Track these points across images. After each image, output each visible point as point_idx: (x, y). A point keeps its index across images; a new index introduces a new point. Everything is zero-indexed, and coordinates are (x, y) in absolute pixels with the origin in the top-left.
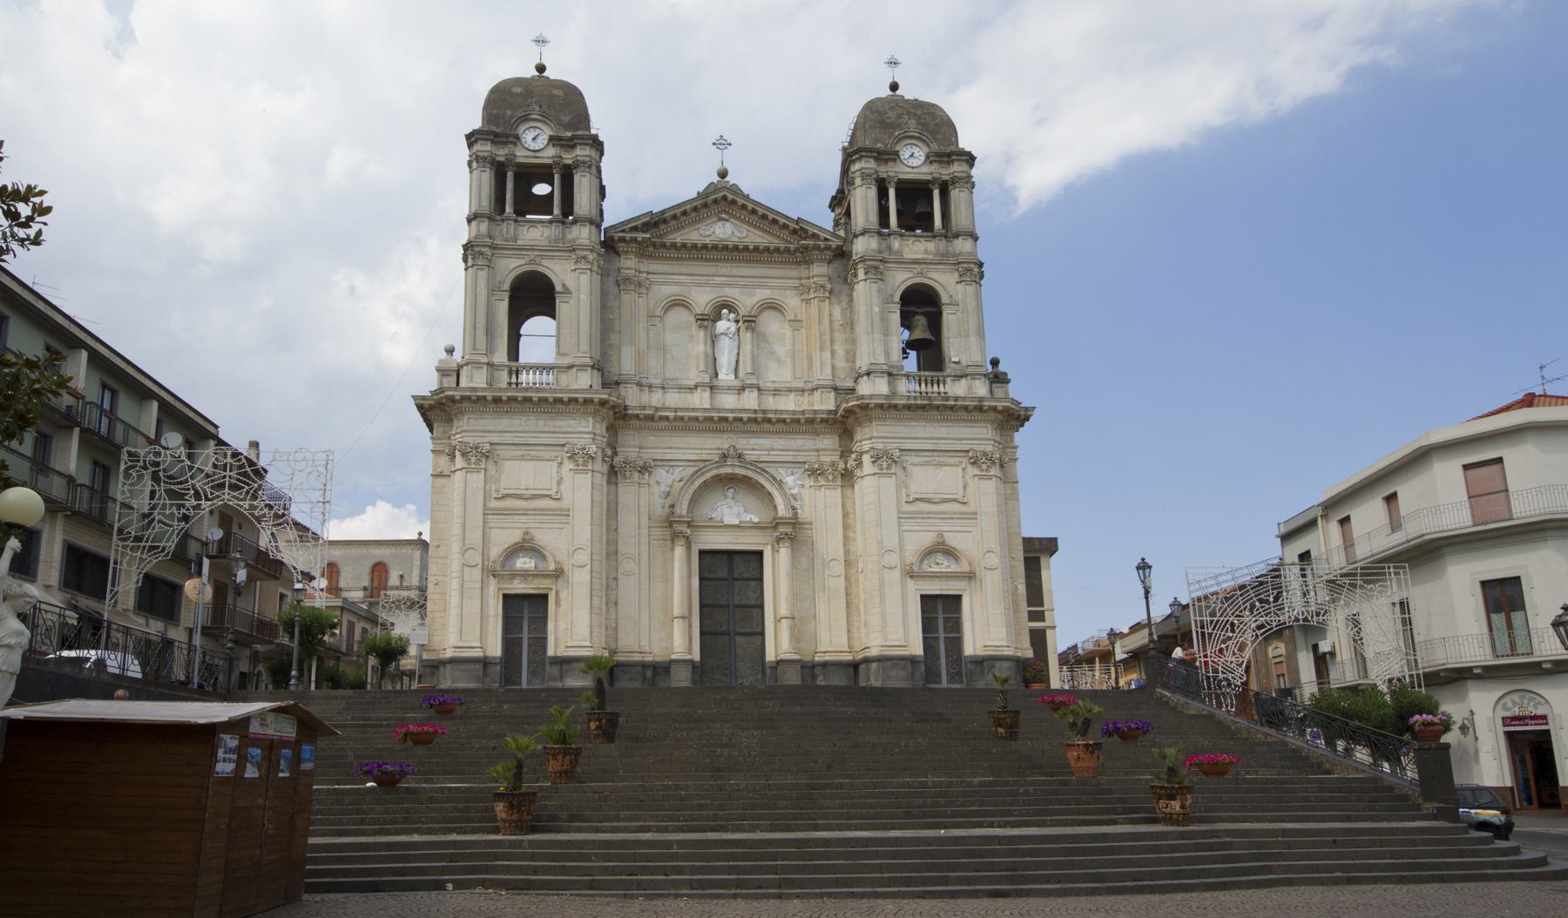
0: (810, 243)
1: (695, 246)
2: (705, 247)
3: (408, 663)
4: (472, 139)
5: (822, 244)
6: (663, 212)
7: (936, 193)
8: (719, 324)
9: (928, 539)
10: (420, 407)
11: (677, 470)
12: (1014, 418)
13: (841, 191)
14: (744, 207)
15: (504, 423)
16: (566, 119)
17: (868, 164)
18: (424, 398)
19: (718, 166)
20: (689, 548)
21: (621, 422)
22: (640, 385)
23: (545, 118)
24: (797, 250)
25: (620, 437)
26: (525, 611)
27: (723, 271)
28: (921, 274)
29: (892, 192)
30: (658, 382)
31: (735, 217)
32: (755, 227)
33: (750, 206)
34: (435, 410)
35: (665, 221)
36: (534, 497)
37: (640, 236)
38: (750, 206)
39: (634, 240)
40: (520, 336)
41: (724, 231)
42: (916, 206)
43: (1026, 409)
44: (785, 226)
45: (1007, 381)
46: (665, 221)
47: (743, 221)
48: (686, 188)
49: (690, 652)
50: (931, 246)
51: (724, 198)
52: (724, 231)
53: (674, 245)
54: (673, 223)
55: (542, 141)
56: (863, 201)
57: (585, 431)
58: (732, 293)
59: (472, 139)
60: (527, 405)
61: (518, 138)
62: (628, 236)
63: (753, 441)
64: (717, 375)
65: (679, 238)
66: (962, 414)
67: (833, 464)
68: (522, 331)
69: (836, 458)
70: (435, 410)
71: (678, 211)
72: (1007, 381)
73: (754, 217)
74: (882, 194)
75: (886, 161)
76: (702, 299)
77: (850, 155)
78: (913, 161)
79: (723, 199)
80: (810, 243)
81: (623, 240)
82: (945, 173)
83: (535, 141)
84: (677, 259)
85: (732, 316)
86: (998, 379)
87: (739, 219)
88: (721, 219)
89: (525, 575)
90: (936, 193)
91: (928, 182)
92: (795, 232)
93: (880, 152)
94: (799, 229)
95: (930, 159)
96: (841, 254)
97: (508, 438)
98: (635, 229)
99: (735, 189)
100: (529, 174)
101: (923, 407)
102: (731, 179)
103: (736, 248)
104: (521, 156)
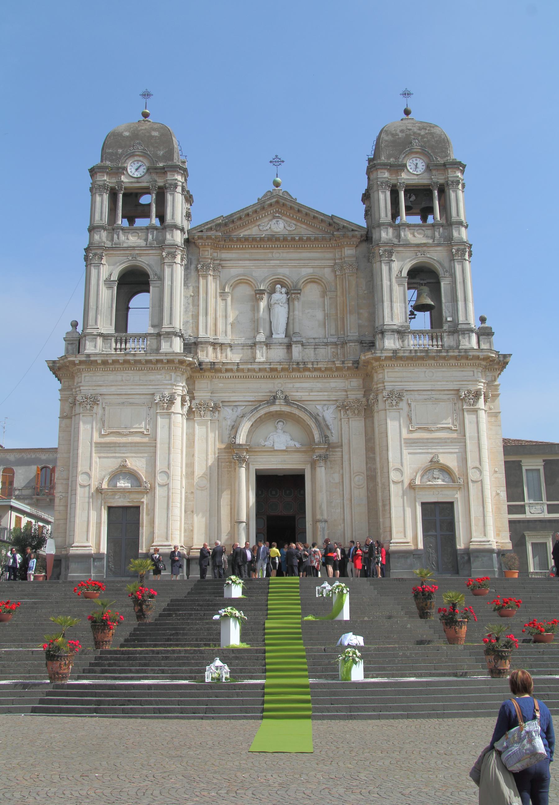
1: (254, 239)
2: (262, 240)
4: (93, 172)
6: (232, 215)
7: (436, 193)
8: (274, 295)
9: (424, 460)
10: (51, 369)
11: (240, 409)
12: (499, 363)
13: (367, 190)
15: (111, 377)
16: (161, 153)
17: (385, 175)
18: (54, 362)
20: (248, 469)
21: (198, 375)
22: (214, 344)
23: (144, 155)
25: (197, 385)
26: (125, 521)
27: (276, 255)
29: (402, 194)
31: (285, 215)
32: (301, 222)
34: (58, 368)
36: (391, 301)
37: (212, 233)
38: (296, 207)
39: (209, 238)
40: (128, 308)
41: (279, 226)
42: (422, 200)
43: (505, 356)
45: (492, 334)
47: (292, 218)
48: (248, 199)
52: (279, 226)
53: (239, 240)
54: (239, 223)
55: (142, 170)
56: (383, 199)
57: (250, 342)
58: (284, 272)
59: (93, 172)
60: (126, 366)
62: (205, 234)
63: (297, 385)
64: (272, 334)
65: (244, 233)
67: (358, 400)
68: (131, 305)
70: (58, 368)
72: (492, 334)
73: (299, 215)
74: (395, 194)
77: (373, 166)
78: (415, 171)
79: (278, 203)
81: (200, 238)
82: (439, 178)
84: (243, 249)
85: (284, 290)
86: (485, 333)
87: (289, 217)
88: (274, 217)
89: (124, 491)
90: (436, 193)
91: (429, 185)
93: (391, 166)
95: (429, 168)
96: (367, 238)
100: (132, 196)
101: (422, 358)
103: (285, 239)
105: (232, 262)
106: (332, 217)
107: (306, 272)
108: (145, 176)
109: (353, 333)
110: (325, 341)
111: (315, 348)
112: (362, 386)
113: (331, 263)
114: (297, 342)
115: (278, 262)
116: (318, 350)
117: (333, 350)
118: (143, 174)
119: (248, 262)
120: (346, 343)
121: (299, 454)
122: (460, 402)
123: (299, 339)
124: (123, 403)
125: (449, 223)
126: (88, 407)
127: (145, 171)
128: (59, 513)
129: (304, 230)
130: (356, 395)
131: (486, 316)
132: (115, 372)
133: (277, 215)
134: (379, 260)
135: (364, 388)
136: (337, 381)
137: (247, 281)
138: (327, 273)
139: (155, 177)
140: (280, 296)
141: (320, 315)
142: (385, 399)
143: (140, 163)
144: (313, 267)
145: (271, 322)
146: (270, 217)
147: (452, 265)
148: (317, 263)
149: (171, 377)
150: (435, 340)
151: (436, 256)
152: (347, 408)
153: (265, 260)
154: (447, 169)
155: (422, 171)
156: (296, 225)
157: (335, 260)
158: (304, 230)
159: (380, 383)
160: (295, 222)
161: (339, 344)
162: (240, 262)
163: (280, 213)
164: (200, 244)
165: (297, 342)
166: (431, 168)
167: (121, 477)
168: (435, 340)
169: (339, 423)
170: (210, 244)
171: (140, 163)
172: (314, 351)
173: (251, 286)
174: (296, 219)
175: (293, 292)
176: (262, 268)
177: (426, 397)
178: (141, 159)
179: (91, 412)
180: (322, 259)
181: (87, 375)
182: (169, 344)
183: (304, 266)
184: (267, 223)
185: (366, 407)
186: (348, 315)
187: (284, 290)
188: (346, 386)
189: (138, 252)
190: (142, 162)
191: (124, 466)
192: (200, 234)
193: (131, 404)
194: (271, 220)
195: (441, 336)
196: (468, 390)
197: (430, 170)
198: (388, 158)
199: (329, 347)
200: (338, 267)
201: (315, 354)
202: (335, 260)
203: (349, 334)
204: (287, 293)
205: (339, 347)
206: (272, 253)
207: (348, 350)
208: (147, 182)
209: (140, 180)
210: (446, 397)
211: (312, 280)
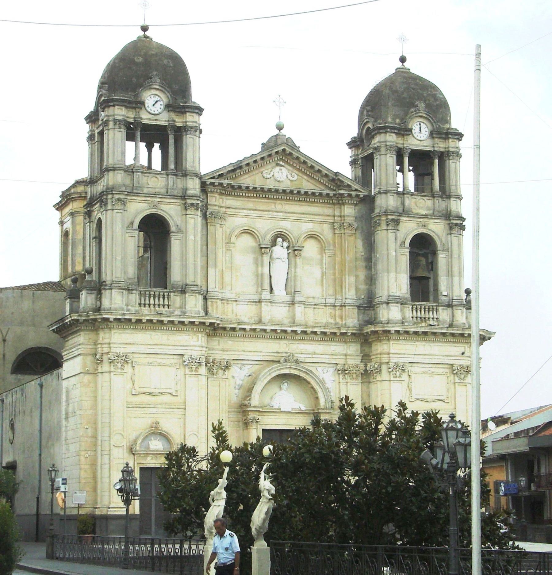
0: (346, 193)
3: (448, 526)
5: (354, 194)
14: (298, 158)
19: (276, 121)
24: (335, 195)
28: (424, 226)
30: (232, 296)
31: (289, 164)
33: (302, 159)
35: (241, 167)
39: (221, 184)
41: (282, 176)
44: (326, 176)
46: (241, 167)
49: (113, 503)
50: (429, 202)
51: (284, 150)
52: (282, 176)
55: (159, 108)
58: (286, 226)
61: (143, 103)
62: (217, 182)
66: (450, 339)
67: (357, 366)
69: (358, 362)
71: (251, 161)
75: (403, 135)
76: (265, 226)
80: (346, 193)
81: (212, 184)
82: (440, 145)
83: (154, 105)
85: (285, 244)
87: (292, 166)
88: (278, 165)
92: (333, 180)
94: (336, 180)
97: (143, 349)
98: (221, 176)
99: (289, 142)
102: (287, 132)
104: (146, 118)
105: (237, 211)
106: (337, 174)
107: (308, 227)
108: (163, 114)
109: (350, 294)
110: (324, 301)
111: (314, 308)
112: (359, 352)
113: (330, 219)
114: (300, 303)
115: (281, 214)
116: (316, 309)
117: (330, 311)
118: (160, 111)
119: (252, 212)
120: (345, 306)
121: (301, 415)
122: (452, 376)
123: (302, 299)
124: (152, 363)
125: (446, 193)
126: (119, 365)
127: (162, 107)
128: (85, 471)
129: (308, 185)
130: (355, 361)
131: (471, 289)
132: (144, 330)
133: (281, 163)
134: (385, 228)
135: (361, 352)
136: (337, 344)
137: (249, 231)
138: (326, 231)
139: (173, 115)
140: (280, 251)
141: (317, 273)
142: (390, 370)
143: (157, 98)
144: (313, 222)
145: (271, 277)
146: (274, 164)
147: (449, 238)
148: (316, 218)
149: (198, 338)
150: (431, 313)
151: (436, 228)
152: (346, 372)
153: (269, 211)
154: (448, 138)
155: (425, 137)
156: (298, 175)
157: (334, 216)
158: (308, 185)
159: (385, 354)
160: (297, 172)
161: (337, 306)
162: (245, 211)
163: (284, 161)
164: (210, 190)
165: (300, 303)
166: (434, 136)
167: (152, 438)
168: (431, 313)
169: (338, 386)
170: (218, 191)
171: (157, 98)
172: (314, 311)
173: (255, 238)
174: (298, 170)
175: (294, 251)
176: (266, 219)
177: (424, 369)
178: (157, 92)
179: (122, 371)
180: (323, 215)
181: (116, 331)
182: (184, 297)
183: (305, 221)
184: (270, 170)
185: (363, 372)
186: (347, 277)
187: (285, 244)
188: (350, 353)
189: (159, 200)
190: (159, 96)
191: (157, 428)
192: (212, 181)
193: (160, 365)
194: (273, 168)
195: (437, 309)
196: (460, 365)
197: (433, 137)
198: (394, 119)
199: (327, 307)
200: (338, 226)
201: (314, 314)
202: (334, 216)
203: (347, 297)
204: (288, 248)
205: (337, 308)
206: (275, 203)
207: (347, 313)
208: (166, 121)
209: (158, 117)
210: (441, 370)
211: (312, 236)
